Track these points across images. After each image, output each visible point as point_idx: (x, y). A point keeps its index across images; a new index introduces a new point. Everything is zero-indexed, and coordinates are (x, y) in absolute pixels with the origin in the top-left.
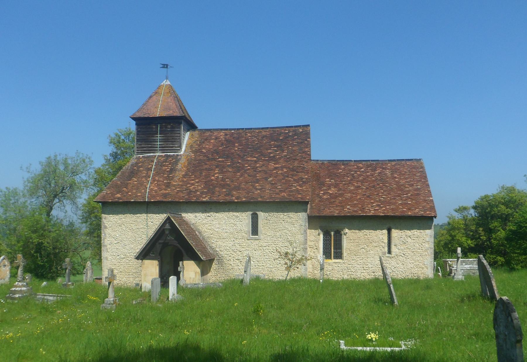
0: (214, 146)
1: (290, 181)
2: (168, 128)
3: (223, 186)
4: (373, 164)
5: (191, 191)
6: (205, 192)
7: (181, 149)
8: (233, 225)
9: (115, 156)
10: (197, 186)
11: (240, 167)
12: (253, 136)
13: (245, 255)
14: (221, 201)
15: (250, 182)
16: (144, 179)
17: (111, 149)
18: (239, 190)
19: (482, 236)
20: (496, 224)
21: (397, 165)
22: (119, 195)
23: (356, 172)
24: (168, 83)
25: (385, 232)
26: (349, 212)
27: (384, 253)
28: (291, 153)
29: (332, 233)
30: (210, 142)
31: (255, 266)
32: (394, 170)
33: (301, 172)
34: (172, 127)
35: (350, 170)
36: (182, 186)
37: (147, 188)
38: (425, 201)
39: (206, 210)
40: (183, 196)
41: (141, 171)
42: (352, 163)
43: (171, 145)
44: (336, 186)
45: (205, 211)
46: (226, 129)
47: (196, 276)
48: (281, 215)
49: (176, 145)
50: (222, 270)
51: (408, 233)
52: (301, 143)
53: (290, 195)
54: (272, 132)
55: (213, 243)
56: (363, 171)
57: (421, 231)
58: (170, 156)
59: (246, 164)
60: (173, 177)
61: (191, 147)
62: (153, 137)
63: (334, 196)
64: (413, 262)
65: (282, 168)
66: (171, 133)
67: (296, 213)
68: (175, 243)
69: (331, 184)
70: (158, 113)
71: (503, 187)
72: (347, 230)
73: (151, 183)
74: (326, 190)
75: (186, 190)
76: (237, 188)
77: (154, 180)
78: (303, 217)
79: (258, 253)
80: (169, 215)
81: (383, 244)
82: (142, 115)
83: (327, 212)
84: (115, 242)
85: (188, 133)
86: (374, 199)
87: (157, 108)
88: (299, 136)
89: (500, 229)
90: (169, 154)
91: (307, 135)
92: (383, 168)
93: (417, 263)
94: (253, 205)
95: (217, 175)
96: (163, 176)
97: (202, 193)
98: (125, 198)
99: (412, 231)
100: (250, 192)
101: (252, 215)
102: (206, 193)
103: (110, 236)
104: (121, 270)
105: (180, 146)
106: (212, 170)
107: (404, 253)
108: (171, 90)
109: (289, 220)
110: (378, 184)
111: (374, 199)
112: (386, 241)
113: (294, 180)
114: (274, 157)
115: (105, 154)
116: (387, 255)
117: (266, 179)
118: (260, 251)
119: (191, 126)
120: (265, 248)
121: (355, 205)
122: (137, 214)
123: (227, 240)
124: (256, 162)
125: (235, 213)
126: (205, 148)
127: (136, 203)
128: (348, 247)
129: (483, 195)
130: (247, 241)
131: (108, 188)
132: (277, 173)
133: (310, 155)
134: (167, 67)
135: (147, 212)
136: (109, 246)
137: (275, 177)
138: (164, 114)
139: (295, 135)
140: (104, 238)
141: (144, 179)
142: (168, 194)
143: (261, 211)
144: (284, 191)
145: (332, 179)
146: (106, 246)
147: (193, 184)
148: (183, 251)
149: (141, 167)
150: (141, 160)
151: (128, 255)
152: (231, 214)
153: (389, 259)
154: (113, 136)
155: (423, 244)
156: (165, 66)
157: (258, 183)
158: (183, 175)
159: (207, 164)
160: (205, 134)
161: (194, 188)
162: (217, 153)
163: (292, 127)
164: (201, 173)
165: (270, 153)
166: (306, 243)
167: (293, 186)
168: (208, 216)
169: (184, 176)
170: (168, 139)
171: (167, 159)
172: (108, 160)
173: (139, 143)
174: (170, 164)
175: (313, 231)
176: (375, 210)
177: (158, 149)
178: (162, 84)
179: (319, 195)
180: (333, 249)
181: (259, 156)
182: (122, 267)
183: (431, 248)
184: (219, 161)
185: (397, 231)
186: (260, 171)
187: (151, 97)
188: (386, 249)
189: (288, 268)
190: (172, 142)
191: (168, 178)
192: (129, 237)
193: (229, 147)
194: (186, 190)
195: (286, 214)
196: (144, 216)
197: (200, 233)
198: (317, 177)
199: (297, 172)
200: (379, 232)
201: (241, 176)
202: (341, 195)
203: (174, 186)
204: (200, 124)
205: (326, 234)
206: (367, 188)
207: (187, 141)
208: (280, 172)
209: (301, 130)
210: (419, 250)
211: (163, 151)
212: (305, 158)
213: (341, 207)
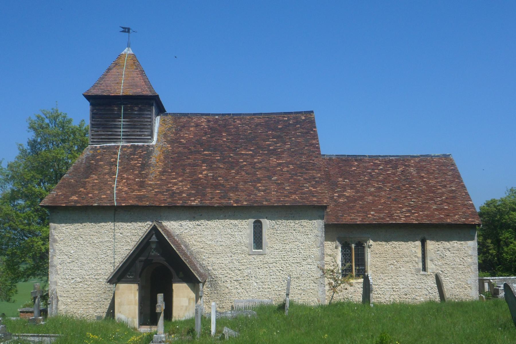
0: (195, 135)
1: (299, 180)
2: (135, 111)
3: (216, 187)
4: (392, 160)
5: (174, 193)
6: (193, 194)
7: (152, 137)
8: (230, 236)
9: (33, 144)
10: (181, 186)
11: (233, 162)
12: (243, 124)
13: (245, 274)
14: (216, 205)
15: (249, 182)
16: (107, 177)
17: (31, 135)
18: (238, 191)
19: (490, 250)
20: (507, 235)
21: (423, 163)
22: (75, 198)
23: (373, 169)
24: (131, 52)
25: (418, 243)
26: (374, 219)
27: (418, 271)
28: (296, 146)
29: (353, 246)
30: (188, 130)
31: (259, 288)
32: (420, 169)
33: (313, 170)
34: (140, 110)
35: (367, 168)
36: (161, 185)
37: (113, 188)
38: (464, 205)
39: (194, 218)
40: (164, 199)
41: (101, 166)
42: (367, 159)
43: (139, 133)
44: (352, 187)
45: (193, 219)
46: (208, 115)
47: (189, 303)
48: (291, 223)
49: (146, 133)
50: (216, 295)
51: (447, 244)
52: (306, 133)
53: (302, 198)
54: (267, 119)
55: (204, 259)
56: (381, 169)
57: (462, 242)
58: (138, 146)
59: (241, 158)
60: (147, 175)
61: (165, 135)
62: (115, 121)
63: (352, 200)
64: (454, 280)
65: (287, 164)
66: (139, 118)
67: (310, 220)
68: (162, 261)
69: (345, 185)
70: (121, 91)
71: (511, 190)
72: (371, 242)
73: (118, 182)
74: (340, 191)
75: (167, 191)
76: (235, 189)
77: (121, 178)
78: (319, 225)
79: (263, 271)
80: (155, 223)
81: (417, 259)
82: (99, 93)
83: (347, 219)
84: (69, 261)
85: (159, 117)
86: (403, 203)
87: (119, 83)
88: (302, 125)
89: (512, 240)
90: (136, 144)
91: (312, 123)
92: (406, 165)
93: (459, 282)
94: (256, 211)
95: (204, 172)
96: (133, 173)
97: (190, 195)
98: (85, 201)
99: (451, 243)
100: (252, 194)
101: (255, 222)
102: (195, 195)
103: (62, 252)
104: (76, 298)
105: (152, 135)
106: (198, 165)
107: (443, 270)
108: (134, 61)
109: (301, 230)
110: (404, 185)
111: (403, 203)
112: (420, 255)
113: (305, 179)
114: (274, 150)
115: (19, 143)
116: (422, 273)
117: (270, 178)
118: (265, 269)
119: (161, 110)
120: (271, 266)
121: (379, 211)
122: (100, 222)
123: (222, 255)
124: (252, 156)
125: (232, 221)
126: (183, 138)
127: (100, 208)
128: (374, 263)
129: (489, 199)
130: (248, 256)
131: (58, 188)
132: (281, 170)
133: (318, 148)
134: (129, 32)
135: (114, 220)
136: (59, 266)
137: (280, 175)
138: (130, 92)
139: (297, 123)
140: (53, 256)
141: (107, 177)
142: (144, 196)
143: (266, 218)
144: (295, 193)
145: (345, 179)
146: (55, 266)
147: (175, 184)
148: (172, 270)
149: (101, 160)
150: (98, 151)
151: (87, 277)
152: (228, 221)
153: (425, 278)
154: (34, 118)
155: (465, 259)
156: (126, 30)
157: (260, 183)
158: (160, 172)
159: (189, 158)
160: (182, 120)
161: (177, 189)
162: (202, 145)
163: (291, 113)
164: (184, 170)
165: (269, 145)
166: (323, 259)
167: (304, 186)
168: (198, 225)
169: (162, 173)
170: (135, 125)
171: (135, 151)
172: (23, 151)
173: (95, 129)
174: (140, 158)
175: (330, 243)
176: (406, 217)
177: (122, 137)
178: (123, 53)
179: (333, 197)
180: (355, 264)
181: (255, 149)
182: (78, 294)
183: (475, 264)
184: (205, 155)
185: (433, 242)
186: (260, 168)
187: (109, 69)
188: (420, 265)
189: (333, 288)
190: (140, 128)
191: (140, 175)
192: (88, 254)
193: (214, 137)
194: (167, 191)
195: (297, 222)
196: (110, 225)
197: (186, 246)
198: (328, 177)
199: (307, 169)
200: (411, 244)
201: (237, 173)
202: (361, 198)
203: (151, 185)
204: (169, 108)
205: (346, 247)
206: (391, 190)
207: (159, 128)
208: (285, 169)
209: (303, 118)
210: (460, 266)
211: (128, 140)
212: (313, 152)
213: (364, 212)
